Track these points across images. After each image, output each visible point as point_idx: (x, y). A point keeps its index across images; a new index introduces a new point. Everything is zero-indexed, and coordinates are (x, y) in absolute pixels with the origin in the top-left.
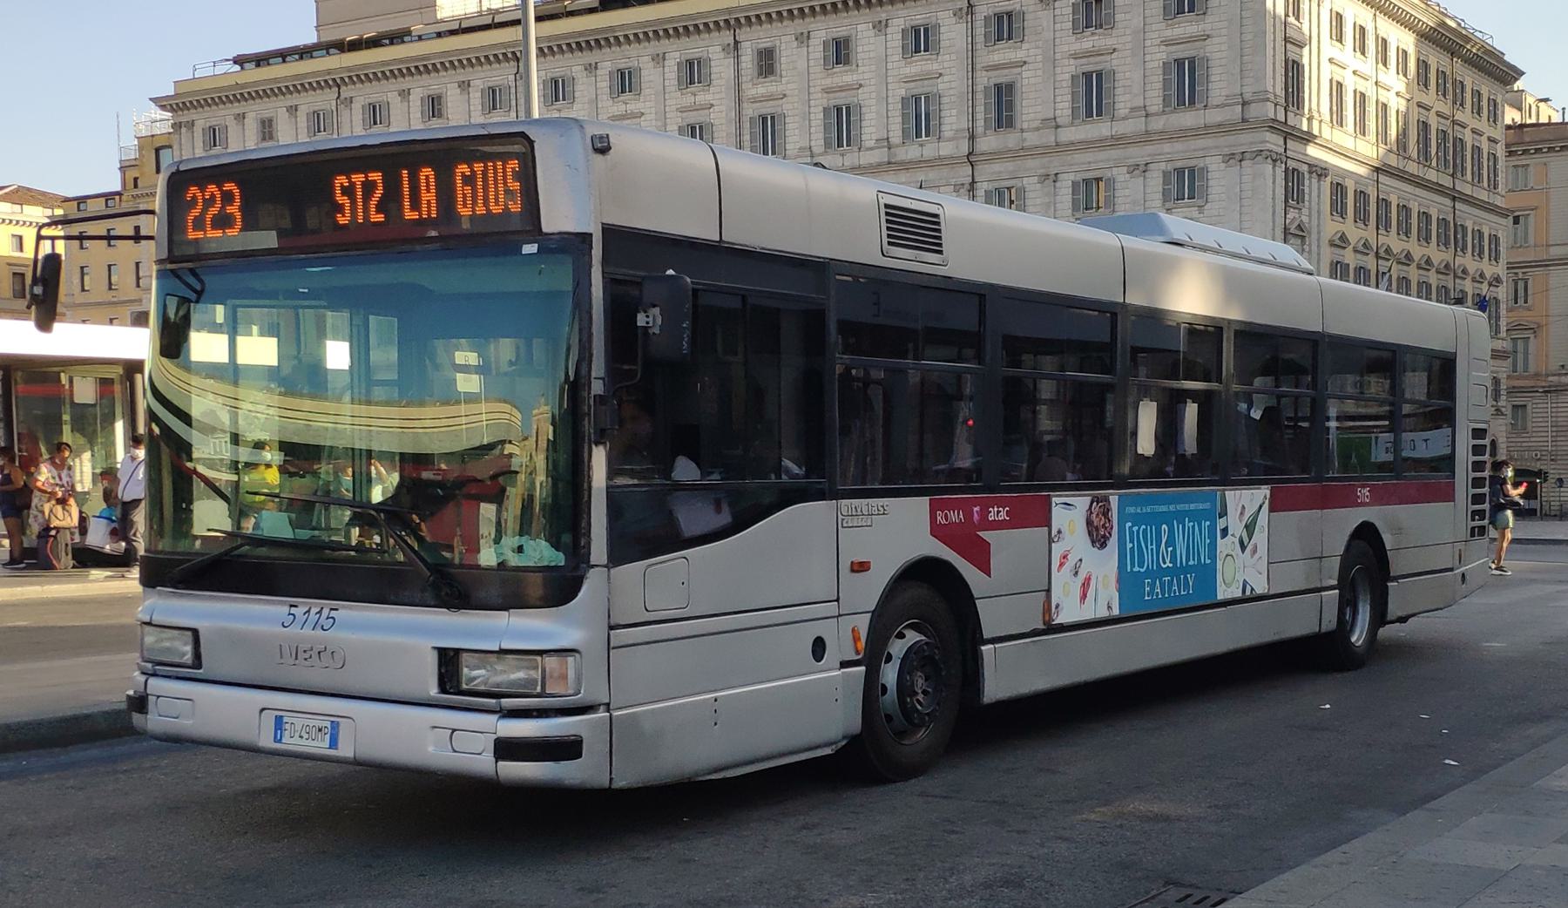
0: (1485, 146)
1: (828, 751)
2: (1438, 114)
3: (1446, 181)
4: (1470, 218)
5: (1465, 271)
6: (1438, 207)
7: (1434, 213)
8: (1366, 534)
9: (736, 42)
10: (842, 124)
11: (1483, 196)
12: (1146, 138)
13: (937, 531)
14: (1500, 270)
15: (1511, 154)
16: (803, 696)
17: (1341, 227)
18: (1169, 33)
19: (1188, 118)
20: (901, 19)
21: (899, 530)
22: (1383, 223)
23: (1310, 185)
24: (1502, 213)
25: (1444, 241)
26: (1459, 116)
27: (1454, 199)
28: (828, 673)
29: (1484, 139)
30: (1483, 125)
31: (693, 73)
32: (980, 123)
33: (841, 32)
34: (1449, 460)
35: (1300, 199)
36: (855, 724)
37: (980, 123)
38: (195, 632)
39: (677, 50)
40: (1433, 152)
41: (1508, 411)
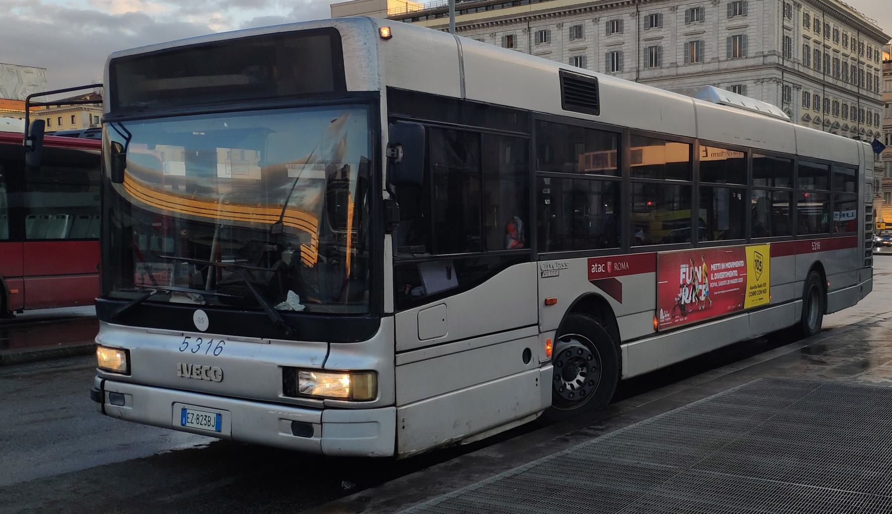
0: (873, 72)
1: (534, 418)
2: (852, 59)
3: (855, 89)
4: (866, 106)
5: (863, 131)
6: (851, 101)
7: (849, 105)
8: (817, 267)
9: (638, 11)
10: (654, 57)
11: (872, 96)
12: (718, 72)
13: (593, 278)
14: (880, 129)
15: (885, 74)
16: (518, 387)
17: (807, 112)
18: (730, 24)
19: (738, 63)
20: (646, 10)
21: (569, 278)
22: (826, 110)
23: (794, 93)
24: (880, 103)
25: (854, 118)
26: (862, 59)
27: (858, 97)
28: (531, 371)
29: (872, 69)
30: (872, 63)
31: (578, 32)
32: (642, 65)
33: (579, 23)
34: (855, 222)
35: (789, 99)
36: (549, 402)
37: (642, 65)
38: (127, 352)
39: (569, 22)
40: (849, 75)
41: (882, 195)
